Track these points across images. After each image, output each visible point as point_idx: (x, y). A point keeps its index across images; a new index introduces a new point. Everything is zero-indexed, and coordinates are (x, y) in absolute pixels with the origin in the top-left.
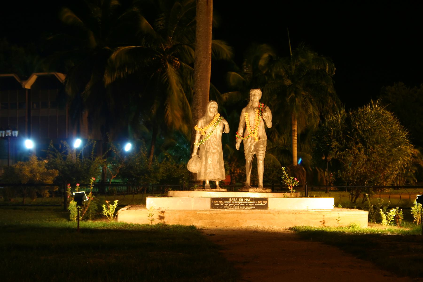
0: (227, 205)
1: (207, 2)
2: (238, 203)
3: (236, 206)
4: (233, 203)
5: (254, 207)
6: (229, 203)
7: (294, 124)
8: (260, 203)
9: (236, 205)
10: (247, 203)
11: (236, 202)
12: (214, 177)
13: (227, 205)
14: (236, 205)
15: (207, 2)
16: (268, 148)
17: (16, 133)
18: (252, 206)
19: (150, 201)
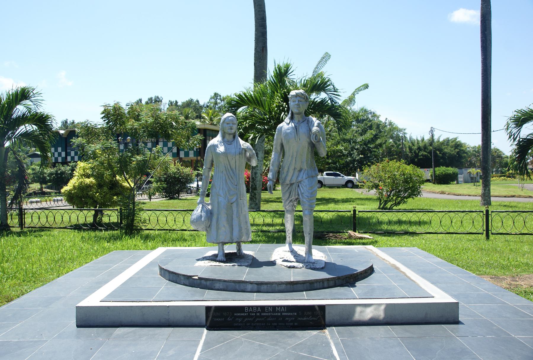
0: (240, 320)
1: (530, 197)
2: (264, 316)
3: (258, 322)
4: (252, 316)
5: (296, 324)
6: (244, 317)
7: (194, 123)
8: (308, 316)
9: (258, 319)
10: (281, 316)
11: (258, 314)
12: (299, 110)
13: (240, 320)
14: (258, 319)
15: (530, 197)
16: (317, 308)
17: (490, 157)
18: (292, 321)
19: (248, 195)
